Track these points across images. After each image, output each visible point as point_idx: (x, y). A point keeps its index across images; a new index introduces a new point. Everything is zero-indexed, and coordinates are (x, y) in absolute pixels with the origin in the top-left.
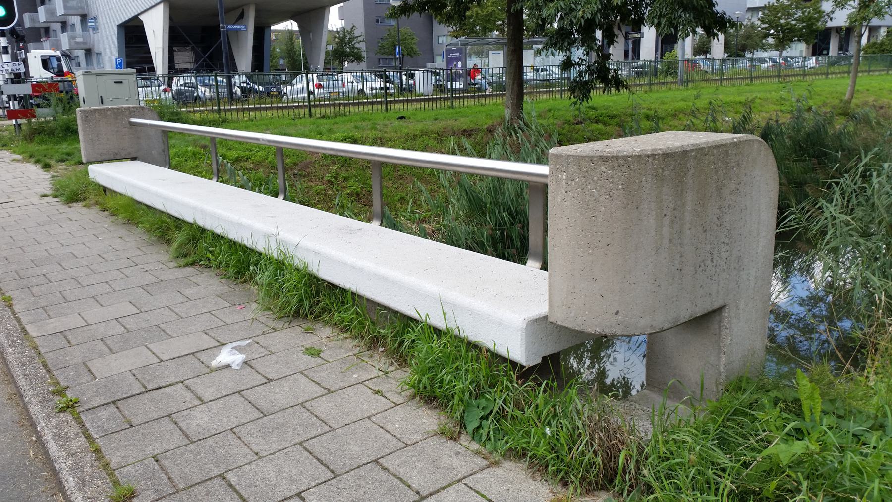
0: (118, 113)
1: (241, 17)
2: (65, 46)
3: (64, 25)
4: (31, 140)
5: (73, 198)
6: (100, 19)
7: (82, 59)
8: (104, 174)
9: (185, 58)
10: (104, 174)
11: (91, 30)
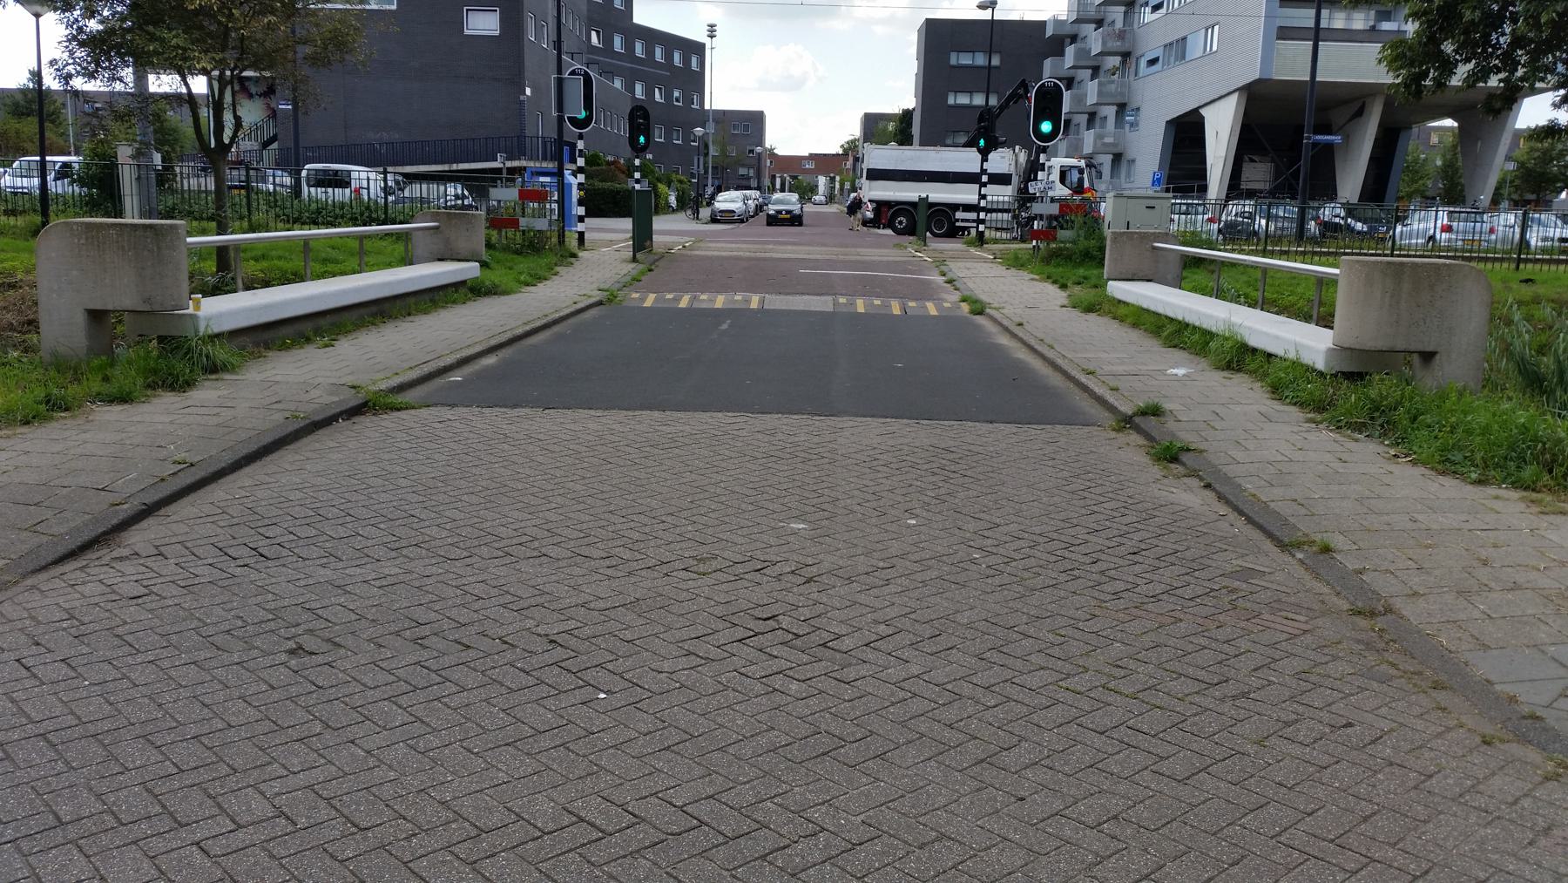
0: (1144, 237)
1: (1360, 113)
2: (1088, 149)
3: (1092, 116)
4: (1048, 263)
5: (1090, 309)
6: (1143, 113)
7: (1106, 170)
8: (1119, 289)
9: (1258, 174)
10: (1119, 289)
11: (1127, 127)
